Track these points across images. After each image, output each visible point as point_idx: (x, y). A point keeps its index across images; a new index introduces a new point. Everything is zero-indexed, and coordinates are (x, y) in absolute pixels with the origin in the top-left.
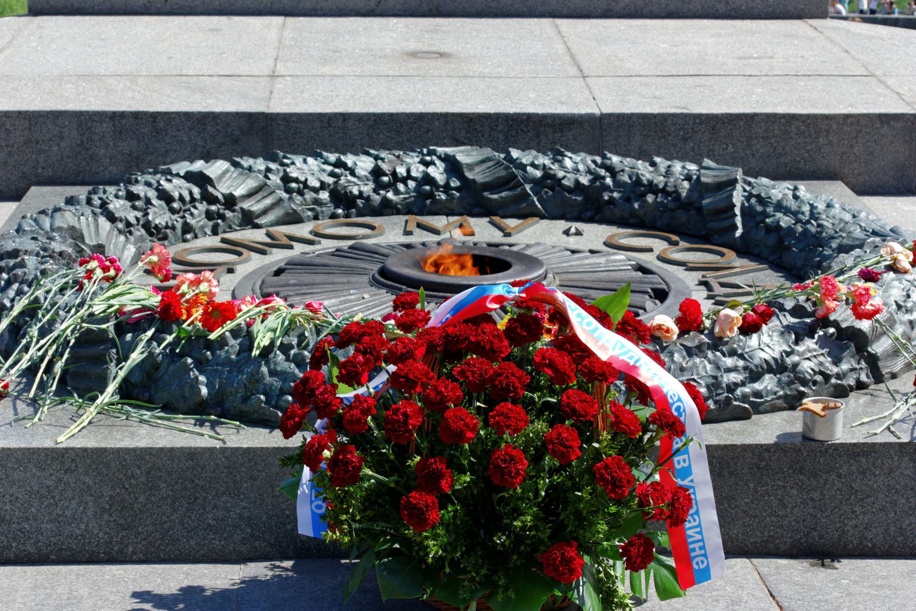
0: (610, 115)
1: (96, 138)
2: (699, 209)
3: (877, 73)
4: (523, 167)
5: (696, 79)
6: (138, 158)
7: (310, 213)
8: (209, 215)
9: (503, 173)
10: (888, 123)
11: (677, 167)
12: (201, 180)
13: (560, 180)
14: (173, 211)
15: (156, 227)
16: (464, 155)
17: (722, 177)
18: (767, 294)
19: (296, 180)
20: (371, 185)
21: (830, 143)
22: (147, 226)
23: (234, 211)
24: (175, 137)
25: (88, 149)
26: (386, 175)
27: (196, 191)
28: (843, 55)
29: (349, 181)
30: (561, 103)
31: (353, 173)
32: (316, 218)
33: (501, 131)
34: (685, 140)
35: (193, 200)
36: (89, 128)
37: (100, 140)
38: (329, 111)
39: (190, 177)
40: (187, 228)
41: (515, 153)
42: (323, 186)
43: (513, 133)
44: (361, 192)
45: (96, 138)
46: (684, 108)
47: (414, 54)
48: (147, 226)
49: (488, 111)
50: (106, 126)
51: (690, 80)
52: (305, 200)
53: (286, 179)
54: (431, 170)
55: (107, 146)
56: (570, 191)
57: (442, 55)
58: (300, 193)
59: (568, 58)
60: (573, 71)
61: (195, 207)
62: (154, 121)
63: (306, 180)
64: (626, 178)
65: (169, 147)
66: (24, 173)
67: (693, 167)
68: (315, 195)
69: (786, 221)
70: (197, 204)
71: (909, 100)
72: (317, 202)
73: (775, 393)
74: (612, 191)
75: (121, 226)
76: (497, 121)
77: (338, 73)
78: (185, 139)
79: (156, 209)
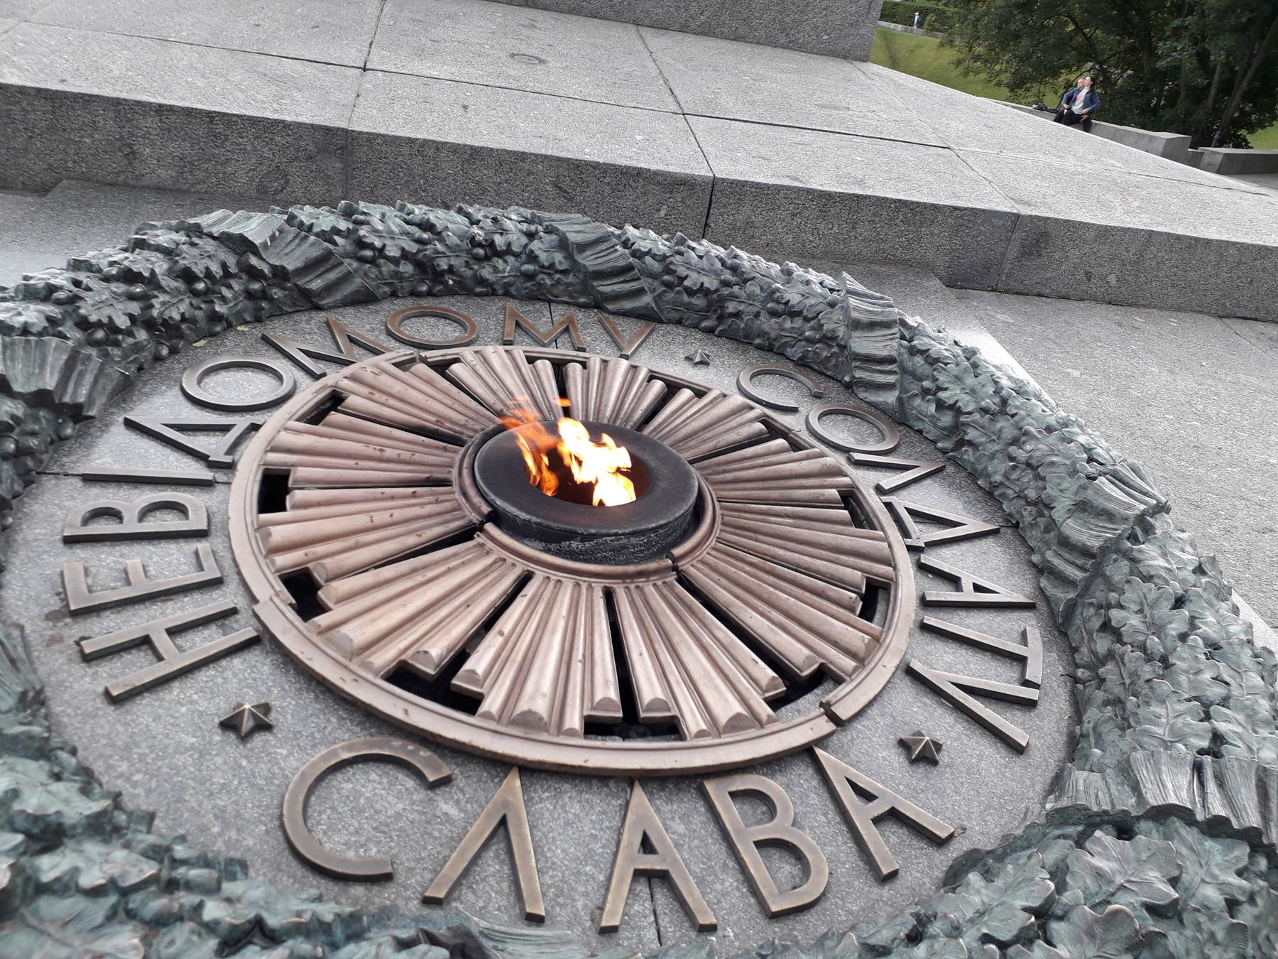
0: (724, 180)
6: (191, 163)
7: (386, 289)
8: (250, 295)
12: (241, 245)
13: (940, 389)
14: (196, 294)
15: (165, 323)
16: (576, 227)
17: (877, 313)
18: (592, 40)
19: (371, 246)
21: (932, 234)
22: (149, 324)
23: (284, 289)
24: (238, 144)
26: (197, 279)
27: (231, 261)
29: (437, 252)
31: (442, 240)
32: (394, 295)
33: (608, 184)
34: (793, 215)
35: (227, 274)
36: (129, 120)
37: (143, 137)
39: (226, 240)
40: (215, 317)
42: (405, 255)
43: (621, 188)
44: (451, 267)
46: (797, 179)
48: (149, 324)
52: (381, 272)
53: (361, 244)
54: (535, 246)
55: (153, 145)
56: (941, 405)
58: (372, 261)
61: (230, 287)
62: (211, 122)
63: (384, 246)
66: (50, 165)
68: (392, 267)
70: (233, 282)
72: (397, 275)
75: (100, 334)
78: (249, 148)
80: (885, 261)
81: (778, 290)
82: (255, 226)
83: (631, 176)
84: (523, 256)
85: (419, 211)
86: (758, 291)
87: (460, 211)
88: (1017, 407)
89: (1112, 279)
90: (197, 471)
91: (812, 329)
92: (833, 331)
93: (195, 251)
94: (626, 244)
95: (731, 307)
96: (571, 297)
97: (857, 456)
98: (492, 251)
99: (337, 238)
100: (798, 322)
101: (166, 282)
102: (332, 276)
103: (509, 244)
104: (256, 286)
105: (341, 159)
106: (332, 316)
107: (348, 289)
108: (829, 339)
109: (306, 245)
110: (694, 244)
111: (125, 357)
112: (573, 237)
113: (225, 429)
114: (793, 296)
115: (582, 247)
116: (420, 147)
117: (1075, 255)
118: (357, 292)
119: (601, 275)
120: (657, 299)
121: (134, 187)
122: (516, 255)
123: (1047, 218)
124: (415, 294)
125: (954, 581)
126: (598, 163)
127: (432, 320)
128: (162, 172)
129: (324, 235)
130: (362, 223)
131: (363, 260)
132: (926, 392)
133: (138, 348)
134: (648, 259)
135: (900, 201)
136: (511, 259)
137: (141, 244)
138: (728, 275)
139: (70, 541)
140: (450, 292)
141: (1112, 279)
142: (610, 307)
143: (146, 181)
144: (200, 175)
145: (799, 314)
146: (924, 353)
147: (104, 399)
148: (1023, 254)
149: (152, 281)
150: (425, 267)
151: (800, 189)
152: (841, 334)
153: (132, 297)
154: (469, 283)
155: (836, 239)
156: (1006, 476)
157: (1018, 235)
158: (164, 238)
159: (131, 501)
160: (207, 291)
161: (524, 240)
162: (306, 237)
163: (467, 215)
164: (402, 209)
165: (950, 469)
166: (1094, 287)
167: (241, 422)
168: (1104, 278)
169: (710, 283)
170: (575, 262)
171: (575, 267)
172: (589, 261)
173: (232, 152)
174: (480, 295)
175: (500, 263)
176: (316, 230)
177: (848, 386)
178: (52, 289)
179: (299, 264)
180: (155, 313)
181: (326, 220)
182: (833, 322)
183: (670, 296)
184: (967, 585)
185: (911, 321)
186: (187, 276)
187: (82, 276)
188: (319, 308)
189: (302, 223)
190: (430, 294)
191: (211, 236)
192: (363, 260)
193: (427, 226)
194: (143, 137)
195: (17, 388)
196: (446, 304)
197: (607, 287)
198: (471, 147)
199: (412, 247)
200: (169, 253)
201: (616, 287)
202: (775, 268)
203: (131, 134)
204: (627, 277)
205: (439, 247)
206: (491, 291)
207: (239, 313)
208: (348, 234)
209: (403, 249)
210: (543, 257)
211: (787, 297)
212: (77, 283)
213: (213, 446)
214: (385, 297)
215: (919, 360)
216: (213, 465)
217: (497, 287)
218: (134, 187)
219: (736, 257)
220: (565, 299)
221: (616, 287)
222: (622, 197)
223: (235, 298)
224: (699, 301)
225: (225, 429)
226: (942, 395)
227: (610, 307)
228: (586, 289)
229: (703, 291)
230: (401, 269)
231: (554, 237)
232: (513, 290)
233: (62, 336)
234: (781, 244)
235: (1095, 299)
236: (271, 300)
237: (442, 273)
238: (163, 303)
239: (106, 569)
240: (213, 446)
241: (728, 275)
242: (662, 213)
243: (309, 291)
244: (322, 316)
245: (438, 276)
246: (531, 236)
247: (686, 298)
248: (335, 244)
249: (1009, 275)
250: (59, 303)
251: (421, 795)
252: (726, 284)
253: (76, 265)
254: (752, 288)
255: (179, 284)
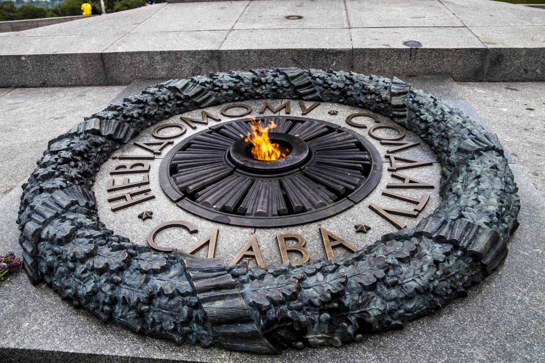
0: (356, 49)
1: (155, 61)
2: (390, 104)
3: (467, 25)
4: (314, 78)
5: (394, 29)
6: (171, 69)
7: (224, 100)
9: (307, 82)
10: (474, 52)
11: (381, 79)
12: (174, 89)
16: (293, 71)
17: (401, 89)
19: (218, 86)
20: (251, 86)
21: (449, 61)
25: (153, 66)
26: (160, 101)
28: (453, 15)
29: (241, 85)
30: (338, 42)
31: (243, 82)
34: (387, 59)
37: (157, 62)
38: (243, 49)
39: (170, 88)
41: (313, 71)
45: (155, 61)
46: (388, 45)
47: (288, 18)
49: (306, 48)
50: (158, 58)
51: (391, 29)
53: (215, 86)
54: (276, 80)
56: (334, 89)
57: (300, 17)
58: (219, 91)
59: (346, 18)
60: (347, 26)
61: (171, 103)
64: (357, 85)
65: (182, 64)
67: (387, 80)
69: (430, 118)
71: (483, 40)
73: (420, 308)
74: (352, 91)
76: (310, 52)
77: (255, 28)
79: (150, 107)
80: (430, 73)
81: (365, 85)
82: (179, 84)
83: (320, 52)
84: (272, 84)
85: (236, 73)
86: (358, 86)
87: (251, 71)
88: (447, 118)
89: (538, 71)
90: (151, 155)
91: (378, 98)
92: (385, 98)
93: (160, 93)
94: (310, 75)
95: (349, 93)
96: (290, 96)
97: (383, 141)
98: (261, 83)
99: (206, 85)
100: (373, 96)
101: (151, 103)
102: (204, 97)
103: (267, 80)
104: (179, 102)
105: (216, 59)
106: (205, 110)
107: (210, 101)
108: (385, 101)
109: (196, 87)
110: (334, 72)
111: (137, 125)
112: (289, 75)
113: (161, 144)
114: (372, 87)
115: (293, 78)
116: (242, 52)
117: (517, 63)
118: (213, 102)
119: (300, 87)
120: (322, 93)
121: (155, 79)
122: (269, 84)
123: (500, 49)
124: (234, 101)
125: (403, 180)
126: (307, 49)
127: (237, 108)
128: (163, 73)
129: (202, 84)
130: (215, 79)
131: (215, 91)
132: (418, 116)
133: (141, 123)
134: (318, 79)
135: (432, 49)
136: (268, 85)
137: (144, 92)
138: (348, 82)
139: (112, 174)
140: (246, 99)
141: (538, 71)
142: (304, 98)
143: (158, 77)
144: (174, 72)
145: (374, 93)
146: (417, 102)
147: (129, 138)
148: (492, 65)
149: (146, 103)
150: (237, 91)
151: (388, 49)
152: (388, 99)
153: (140, 108)
154: (253, 95)
155: (407, 67)
156: (439, 144)
157: (488, 57)
158: (152, 90)
159: (129, 163)
160: (163, 105)
161: (272, 78)
162: (196, 85)
163: (254, 72)
164: (230, 73)
165: (422, 144)
166: (529, 75)
167: (166, 141)
168: (534, 71)
169: (341, 85)
170: (291, 83)
171: (292, 85)
172: (296, 83)
173: (183, 63)
174: (257, 99)
175: (264, 87)
176: (200, 82)
177: (392, 118)
178: (117, 107)
179: (193, 94)
180: (146, 112)
181: (204, 79)
182: (385, 94)
183: (326, 91)
184: (407, 181)
185: (415, 91)
186: (157, 100)
187: (126, 103)
188: (201, 108)
189: (195, 81)
190: (239, 100)
191: (166, 87)
192: (215, 91)
193: (238, 77)
194: (157, 62)
195: (103, 134)
196: (244, 103)
197: (302, 91)
198: (260, 50)
199: (233, 85)
200: (153, 94)
201: (305, 91)
202: (367, 78)
203: (153, 62)
204: (309, 87)
205: (241, 83)
206: (261, 97)
207: (174, 112)
208: (211, 82)
209: (229, 86)
210: (279, 83)
211: (369, 87)
212: (124, 105)
213: (156, 148)
214: (223, 103)
215: (415, 105)
216: (155, 153)
217: (263, 96)
218: (155, 79)
219: (352, 75)
220: (288, 97)
221: (305, 91)
222: (317, 60)
223: (173, 106)
224: (337, 93)
225: (161, 144)
226: (422, 117)
227: (304, 98)
228: (296, 93)
229: (338, 88)
230: (229, 92)
231: (283, 76)
232: (269, 96)
233: (117, 120)
234: (384, 71)
235: (531, 80)
236: (184, 106)
237: (244, 92)
238: (149, 109)
239: (120, 180)
240: (156, 148)
241: (348, 82)
242: (334, 64)
243: (197, 102)
244: (201, 110)
245: (242, 94)
246: (275, 76)
247: (332, 91)
248: (206, 86)
249: (487, 74)
250: (118, 111)
251: (188, 235)
252: (347, 85)
253: (125, 100)
254: (357, 85)
255: (155, 103)
